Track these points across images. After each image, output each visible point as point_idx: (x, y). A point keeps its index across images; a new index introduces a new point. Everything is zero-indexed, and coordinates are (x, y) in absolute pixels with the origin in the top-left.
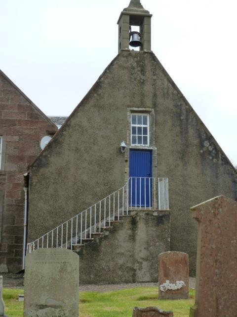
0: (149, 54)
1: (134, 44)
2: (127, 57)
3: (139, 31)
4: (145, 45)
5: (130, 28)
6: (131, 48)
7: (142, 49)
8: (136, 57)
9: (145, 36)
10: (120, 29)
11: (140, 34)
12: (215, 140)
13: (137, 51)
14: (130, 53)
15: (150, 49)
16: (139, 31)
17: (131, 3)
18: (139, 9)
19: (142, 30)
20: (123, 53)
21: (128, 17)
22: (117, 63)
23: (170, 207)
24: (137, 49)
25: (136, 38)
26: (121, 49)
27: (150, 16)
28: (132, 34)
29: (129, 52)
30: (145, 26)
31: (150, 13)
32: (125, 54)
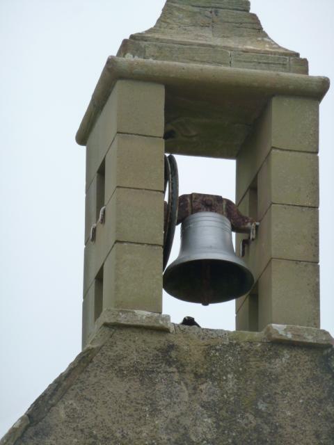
0: (304, 357)
1: (198, 280)
2: (144, 374)
3: (230, 194)
4: (279, 290)
5: (170, 172)
6: (175, 309)
7: (251, 317)
8: (209, 376)
9: (279, 228)
10: (98, 177)
11: (243, 215)
12: (319, 322)
13: (229, 333)
14: (172, 347)
15: (317, 324)
16: (230, 194)
17: (167, 11)
18: (231, 43)
19: (250, 185)
20: (117, 337)
21: (156, 98)
22: (72, 416)
23: (184, 197)
24: (220, 316)
25: (213, 240)
26: (105, 317)
27: (317, 91)
28: (184, 210)
29: (155, 341)
30: (276, 156)
31: (315, 71)
32: (135, 349)
